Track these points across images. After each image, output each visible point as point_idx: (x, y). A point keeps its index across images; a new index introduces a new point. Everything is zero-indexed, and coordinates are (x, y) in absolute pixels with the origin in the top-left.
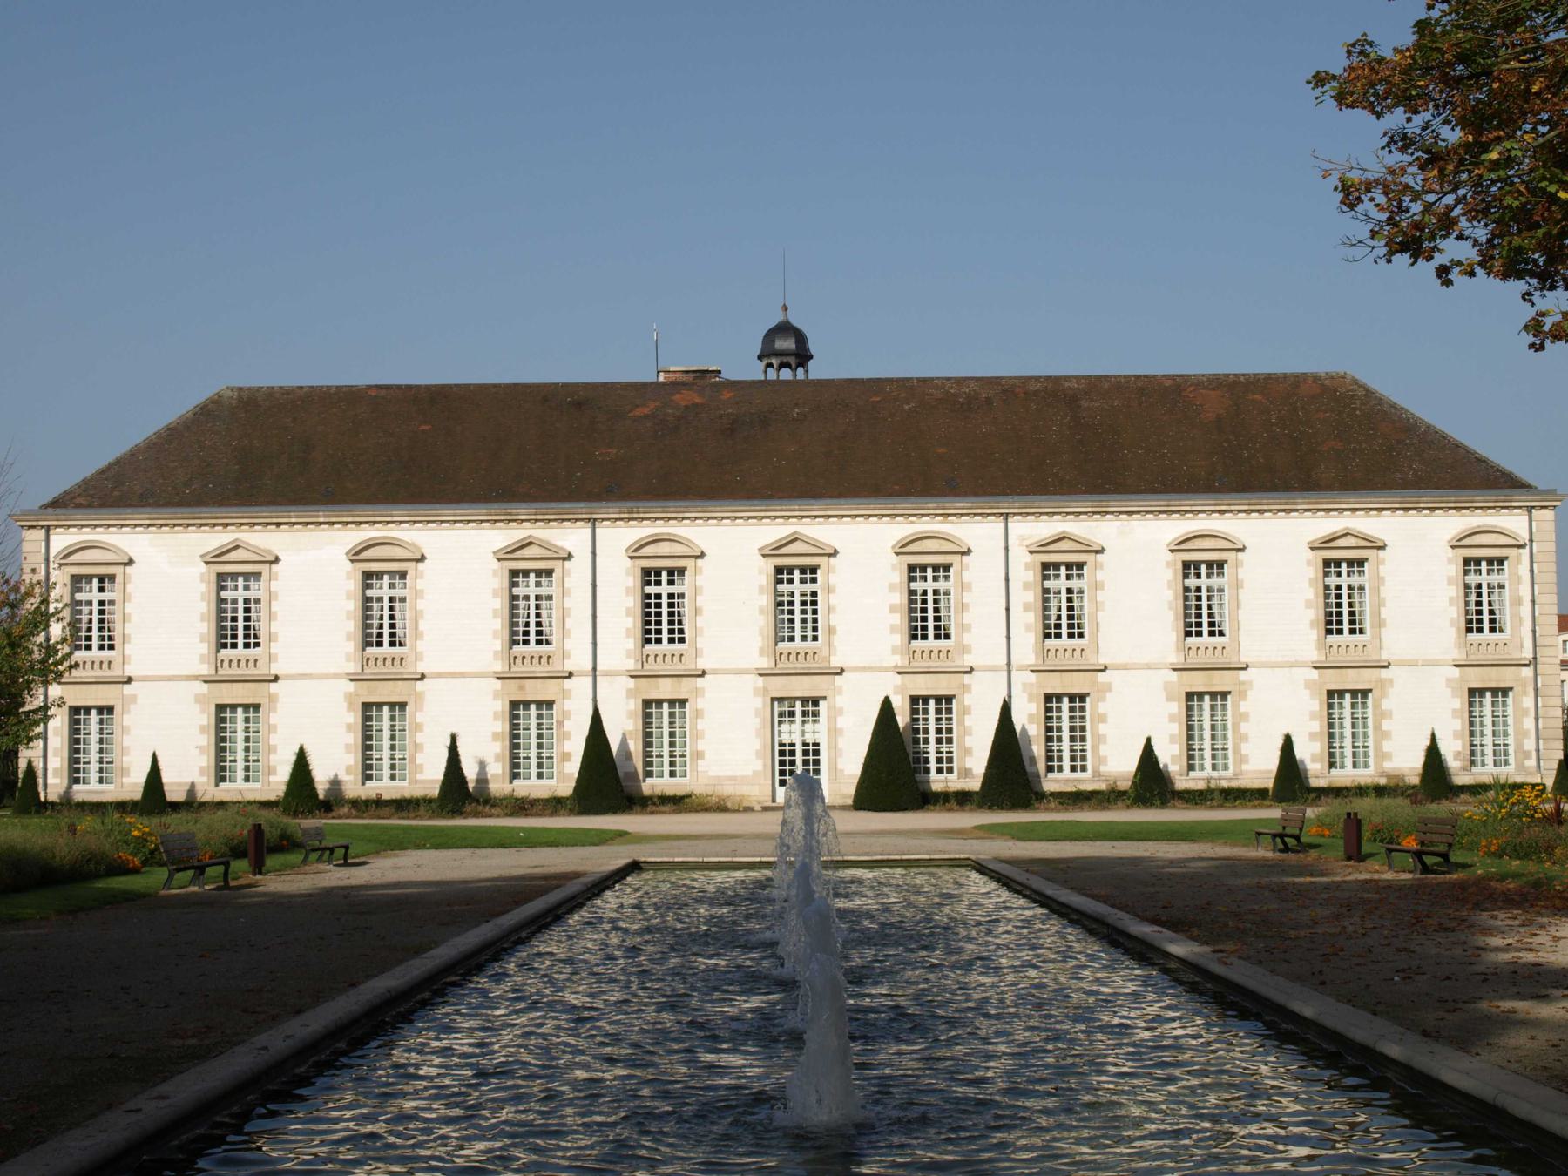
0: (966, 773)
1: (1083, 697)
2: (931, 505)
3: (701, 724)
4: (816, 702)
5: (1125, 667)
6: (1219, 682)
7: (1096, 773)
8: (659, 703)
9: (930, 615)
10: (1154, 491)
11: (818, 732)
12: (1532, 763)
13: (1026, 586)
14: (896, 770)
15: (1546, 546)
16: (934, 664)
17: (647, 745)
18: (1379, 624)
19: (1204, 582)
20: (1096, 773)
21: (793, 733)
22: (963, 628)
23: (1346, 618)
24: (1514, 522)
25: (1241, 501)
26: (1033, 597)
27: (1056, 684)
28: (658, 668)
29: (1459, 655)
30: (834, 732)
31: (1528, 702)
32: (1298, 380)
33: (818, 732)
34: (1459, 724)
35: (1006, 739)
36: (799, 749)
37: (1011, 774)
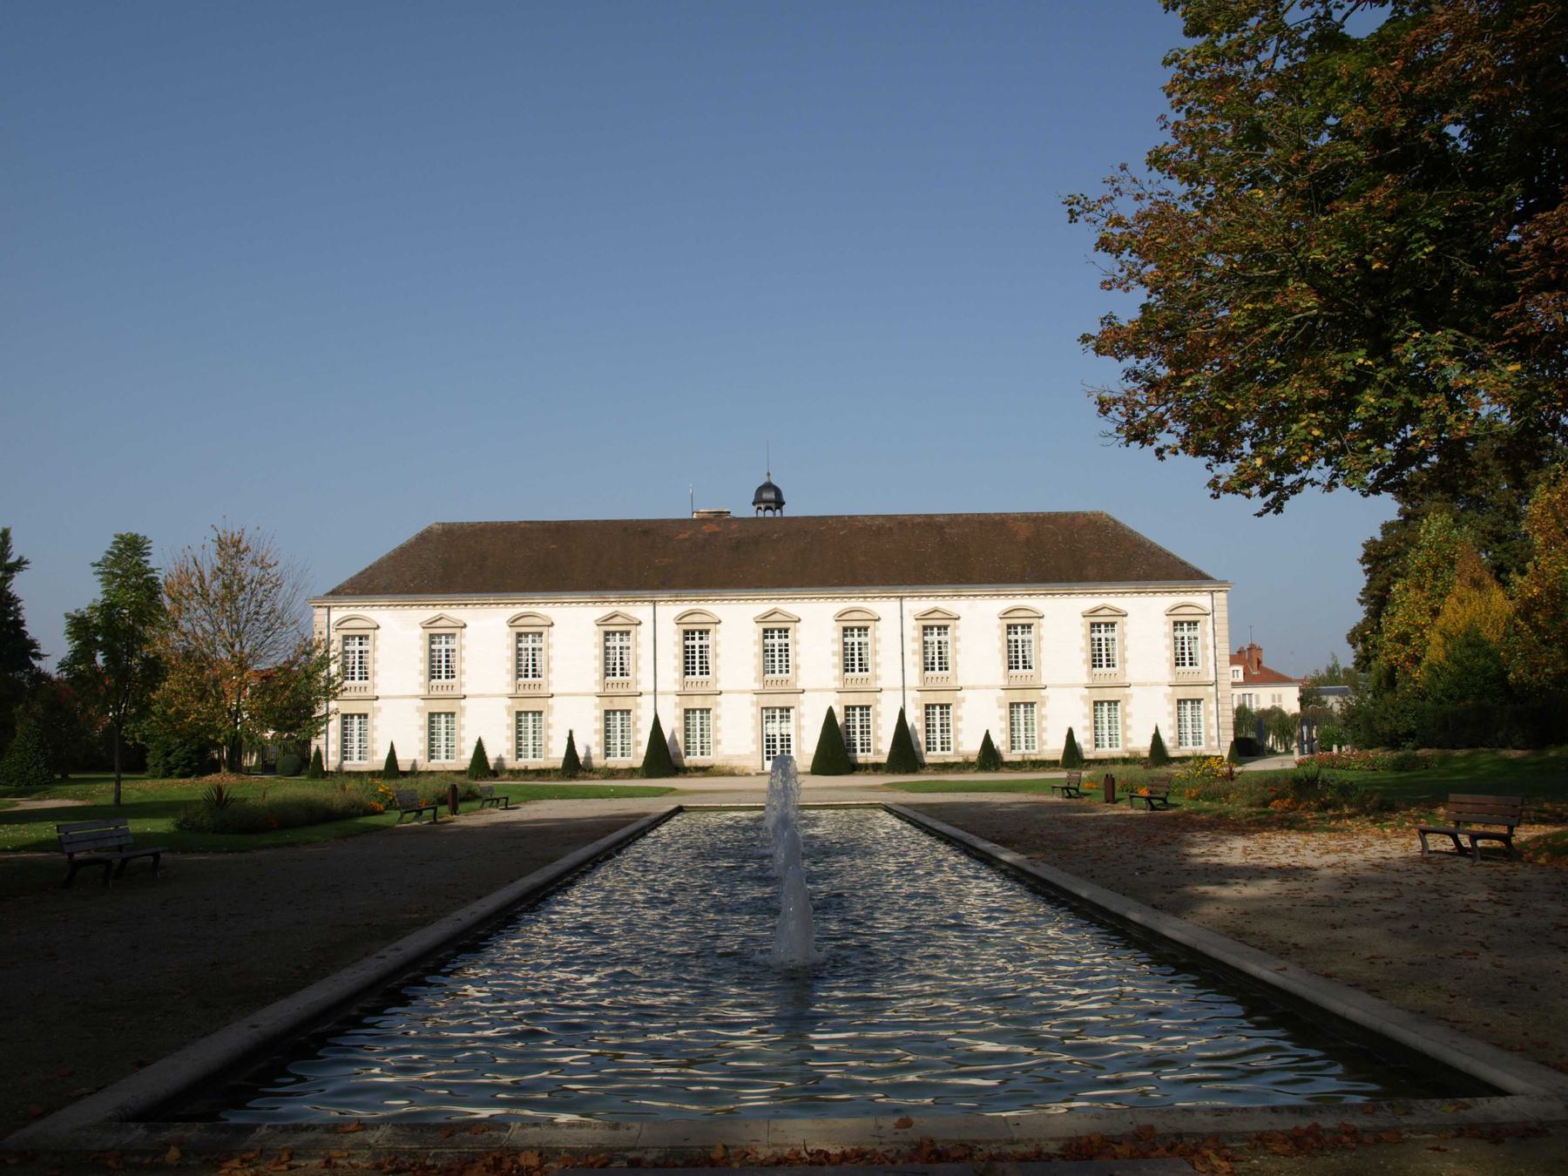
0: (878, 752)
1: (948, 706)
2: (857, 592)
3: (719, 723)
4: (788, 710)
5: (973, 688)
6: (1029, 696)
7: (956, 752)
8: (694, 711)
10: (990, 583)
11: (789, 728)
12: (1215, 743)
13: (914, 640)
14: (836, 750)
15: (1222, 614)
16: (859, 687)
17: (687, 736)
18: (1124, 661)
19: (1020, 637)
20: (956, 752)
21: (775, 728)
23: (857, 662)
24: (1202, 600)
26: (918, 646)
27: (932, 698)
28: (615, 690)
29: (1171, 679)
31: (1213, 707)
32: (1074, 517)
33: (789, 728)
34: (1172, 721)
35: (902, 728)
36: (778, 738)
37: (905, 752)
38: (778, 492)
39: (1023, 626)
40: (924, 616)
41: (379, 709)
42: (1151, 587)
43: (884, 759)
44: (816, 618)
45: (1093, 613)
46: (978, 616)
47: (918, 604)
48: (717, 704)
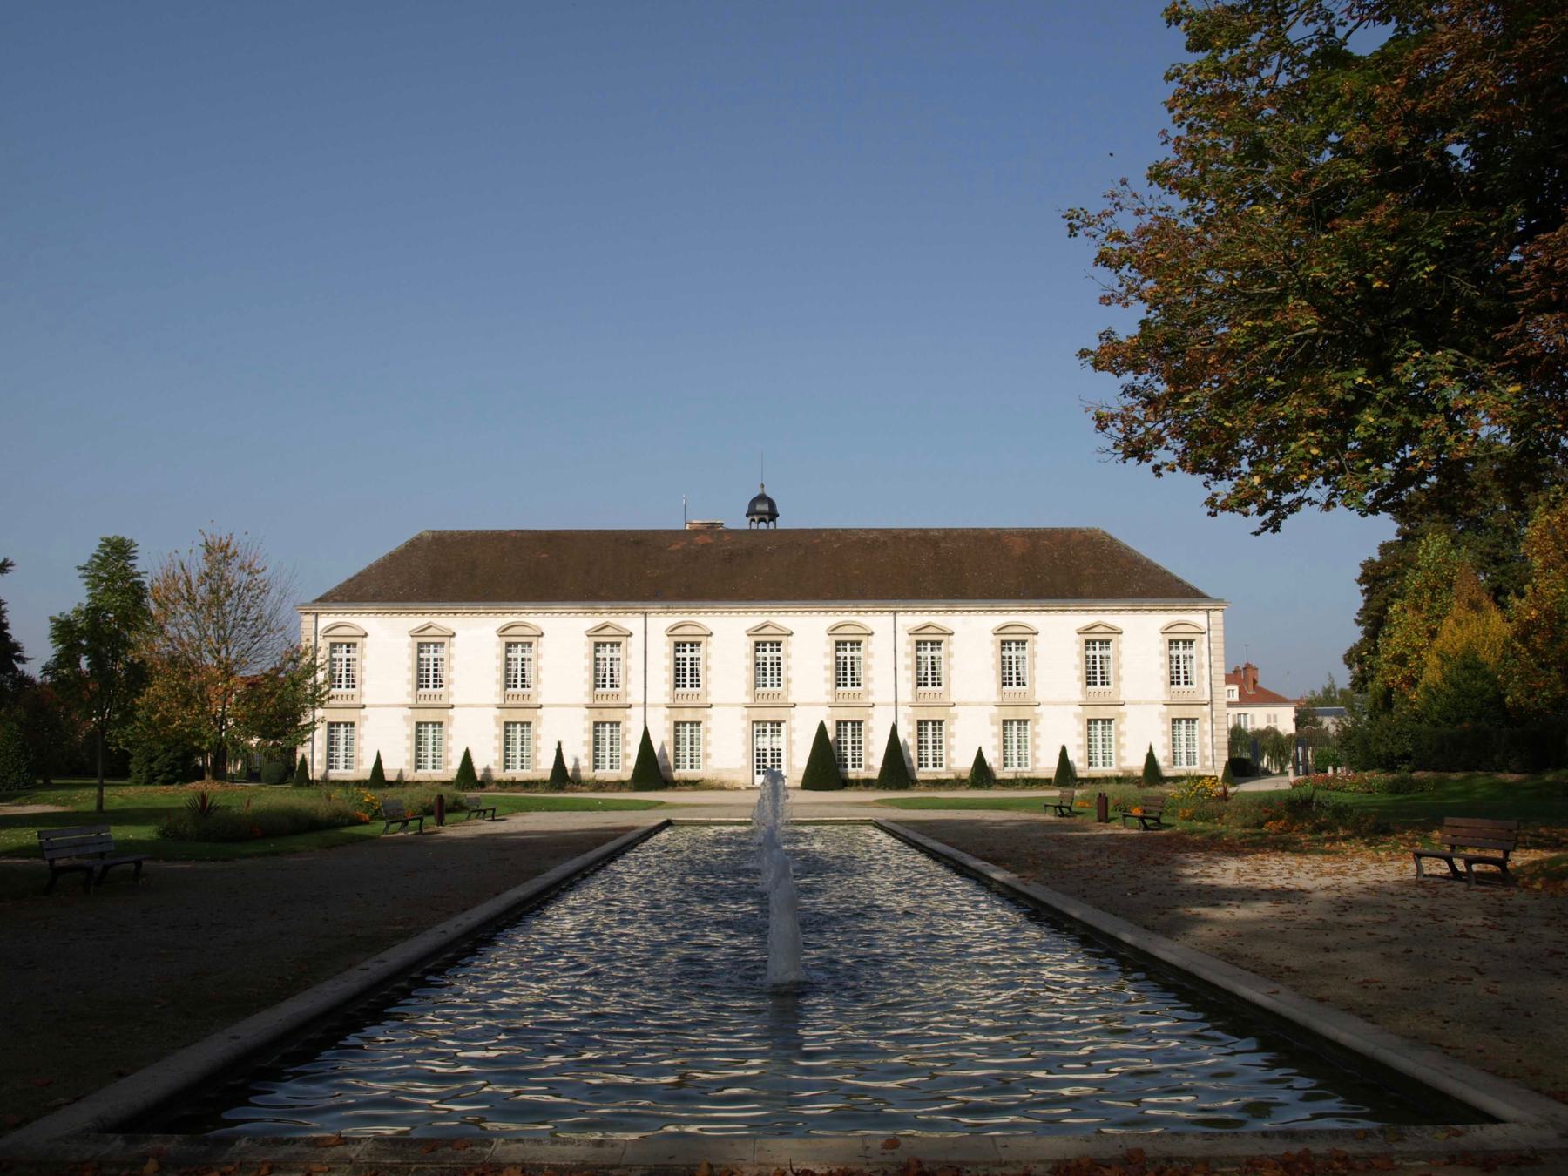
0: (870, 768)
2: (850, 606)
4: (779, 724)
5: (966, 704)
6: (1023, 713)
7: (949, 768)
8: (684, 724)
9: (849, 671)
11: (781, 742)
12: (1209, 763)
14: (827, 765)
15: (1218, 633)
16: (851, 702)
17: (677, 749)
18: (1119, 679)
19: (1014, 653)
20: (949, 768)
21: (765, 742)
22: (789, 681)
24: (1198, 618)
25: (1035, 605)
26: (911, 661)
27: (924, 714)
29: (1167, 699)
30: (790, 742)
31: (1207, 727)
33: (781, 742)
35: (894, 748)
36: (769, 752)
38: (772, 504)
39: (1017, 643)
40: (918, 631)
41: (366, 718)
42: (1147, 604)
43: (875, 775)
44: (808, 631)
45: (1088, 630)
46: (973, 631)
47: (912, 619)
48: (707, 717)
